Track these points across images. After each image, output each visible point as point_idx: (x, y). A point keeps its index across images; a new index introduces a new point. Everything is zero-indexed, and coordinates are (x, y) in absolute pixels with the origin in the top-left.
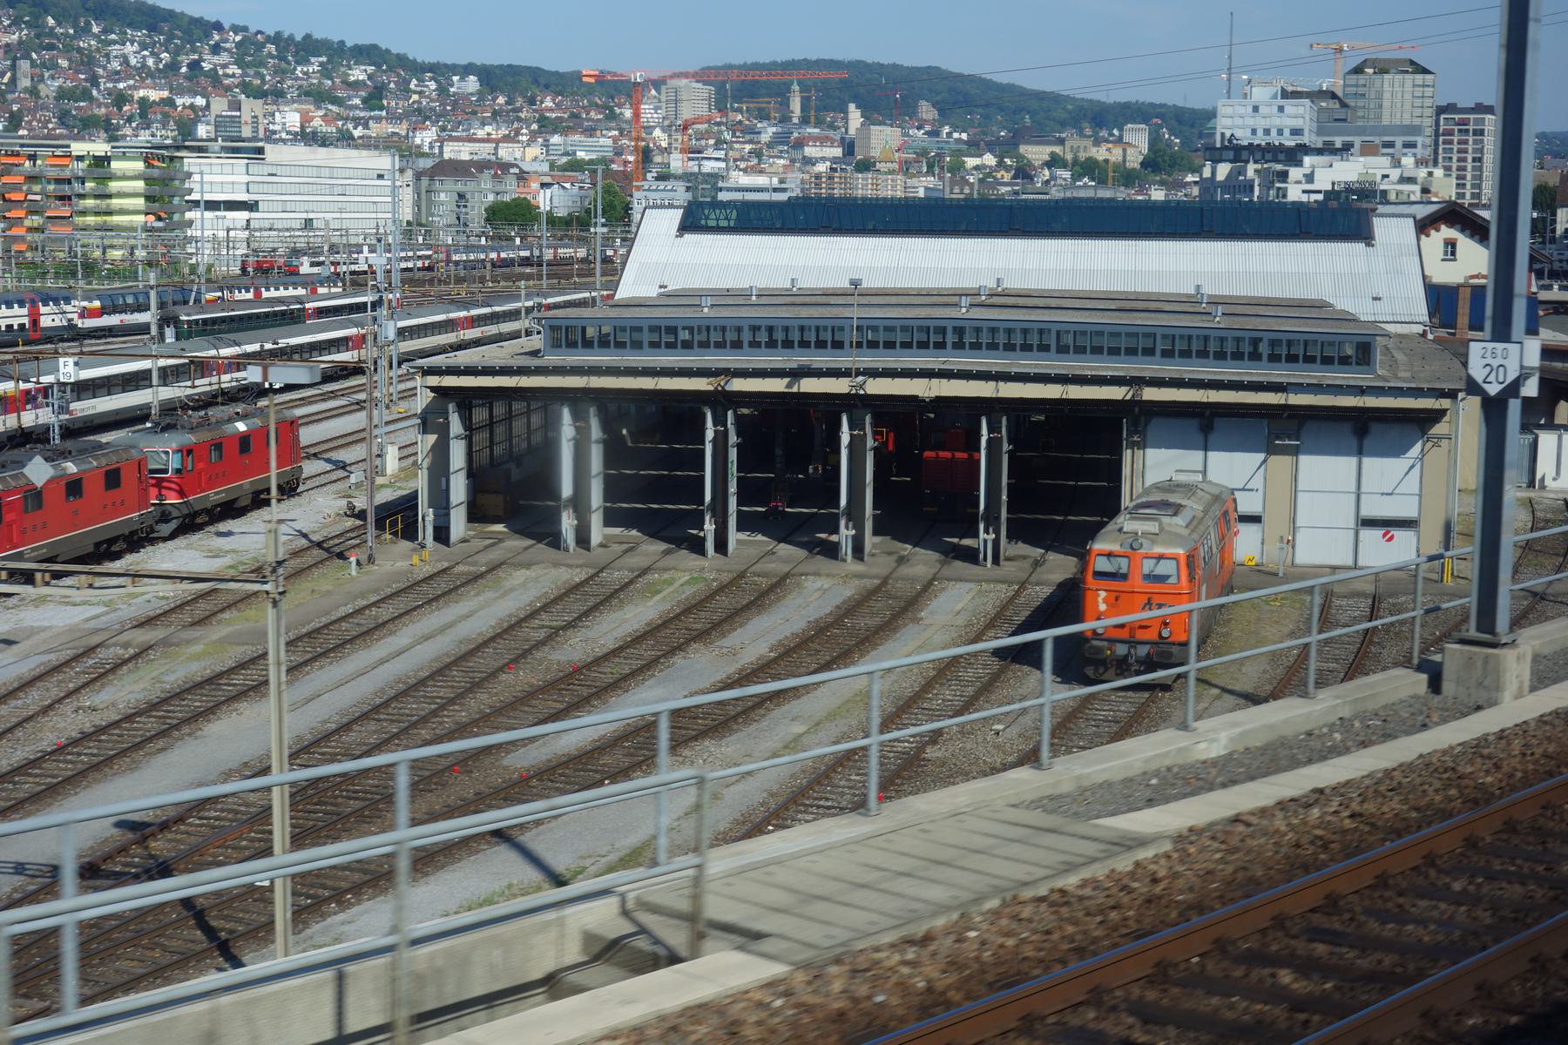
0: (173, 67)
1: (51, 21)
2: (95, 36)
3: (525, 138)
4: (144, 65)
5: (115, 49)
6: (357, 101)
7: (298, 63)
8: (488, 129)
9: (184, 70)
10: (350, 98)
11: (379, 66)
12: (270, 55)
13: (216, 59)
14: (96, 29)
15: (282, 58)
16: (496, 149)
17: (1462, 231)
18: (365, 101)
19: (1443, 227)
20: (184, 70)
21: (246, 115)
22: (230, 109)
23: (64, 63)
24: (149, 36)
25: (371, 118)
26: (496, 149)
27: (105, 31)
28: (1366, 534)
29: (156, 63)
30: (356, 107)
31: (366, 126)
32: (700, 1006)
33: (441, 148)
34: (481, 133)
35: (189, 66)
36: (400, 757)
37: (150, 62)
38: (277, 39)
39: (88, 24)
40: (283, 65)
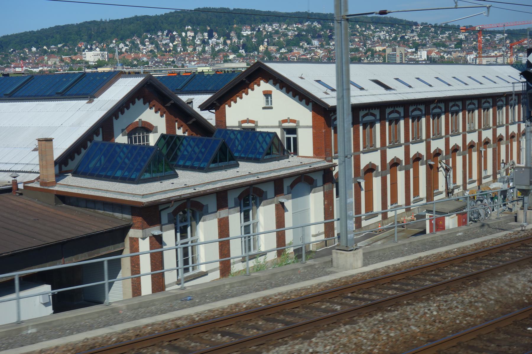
0: (395, 38)
1: (358, 26)
2: (372, 30)
3: (509, 55)
4: (385, 38)
5: (377, 34)
6: (453, 46)
7: (441, 34)
8: (496, 52)
9: (399, 39)
10: (450, 45)
11: (470, 33)
12: (432, 32)
13: (412, 35)
14: (372, 28)
15: (436, 32)
16: (496, 59)
17: (274, 84)
18: (455, 45)
19: (262, 82)
20: (399, 39)
21: (398, 53)
22: (393, 51)
23: (357, 40)
24: (390, 29)
25: (452, 51)
26: (496, 59)
27: (376, 28)
28: (175, 250)
29: (389, 38)
30: (452, 48)
31: (451, 54)
32: (452, 244)
33: (476, 60)
34: (493, 54)
35: (401, 38)
36: (105, 259)
37: (387, 37)
38: (435, 26)
39: (370, 26)
40: (435, 35)
